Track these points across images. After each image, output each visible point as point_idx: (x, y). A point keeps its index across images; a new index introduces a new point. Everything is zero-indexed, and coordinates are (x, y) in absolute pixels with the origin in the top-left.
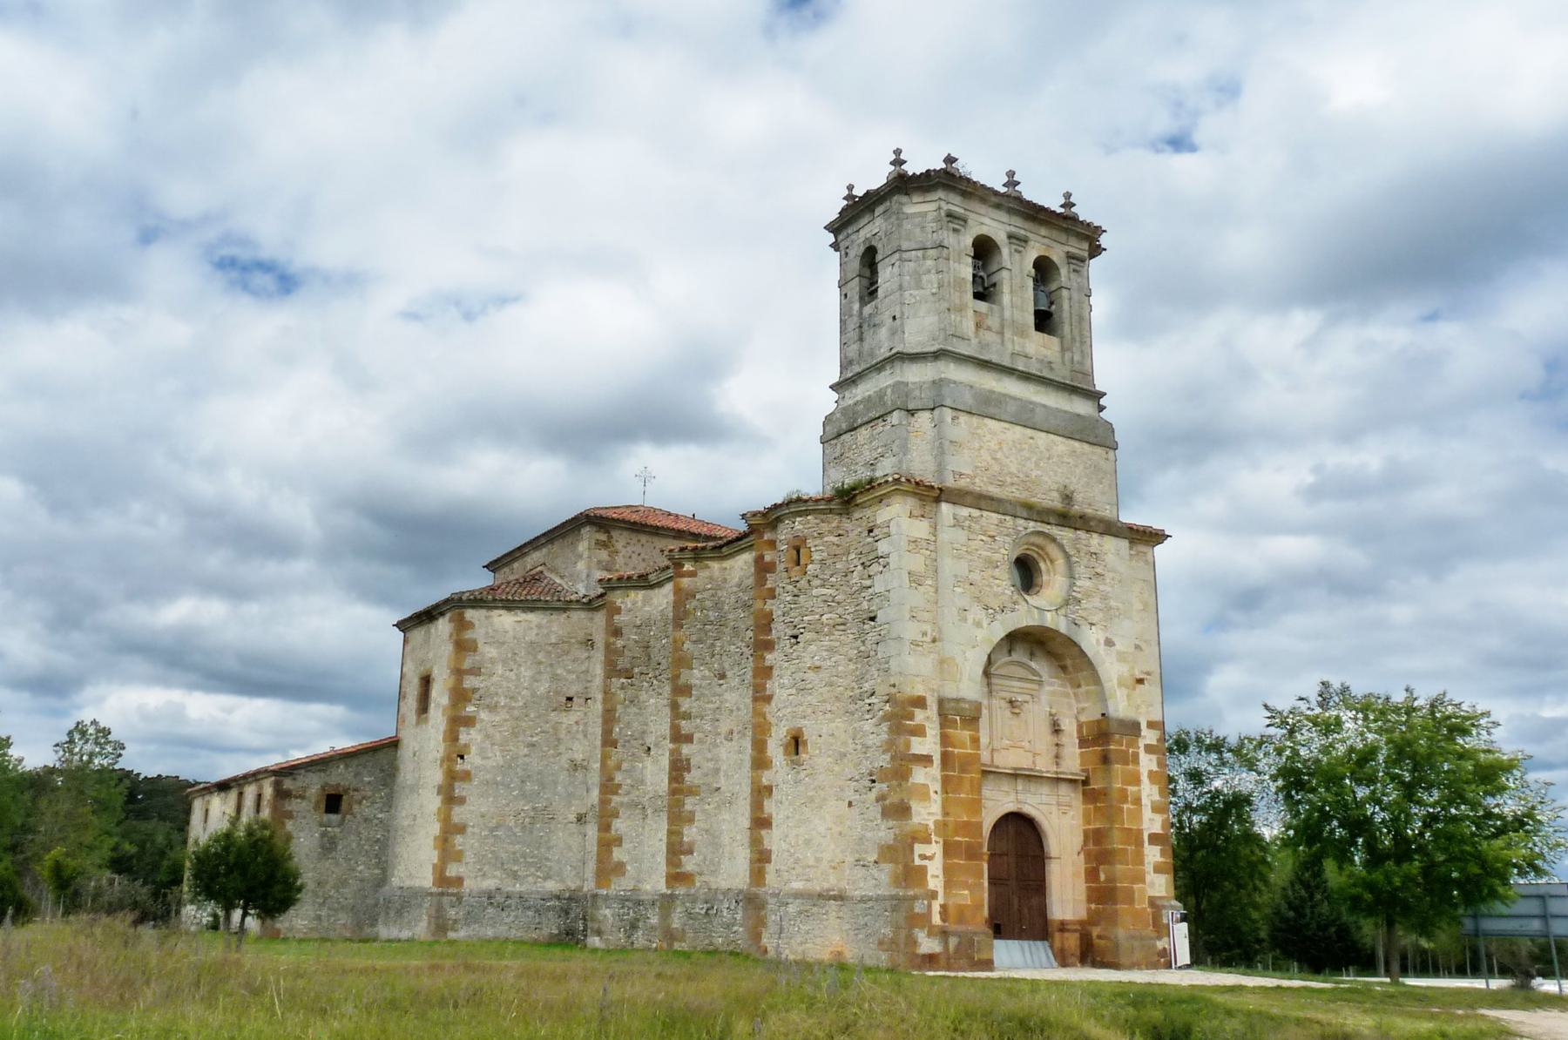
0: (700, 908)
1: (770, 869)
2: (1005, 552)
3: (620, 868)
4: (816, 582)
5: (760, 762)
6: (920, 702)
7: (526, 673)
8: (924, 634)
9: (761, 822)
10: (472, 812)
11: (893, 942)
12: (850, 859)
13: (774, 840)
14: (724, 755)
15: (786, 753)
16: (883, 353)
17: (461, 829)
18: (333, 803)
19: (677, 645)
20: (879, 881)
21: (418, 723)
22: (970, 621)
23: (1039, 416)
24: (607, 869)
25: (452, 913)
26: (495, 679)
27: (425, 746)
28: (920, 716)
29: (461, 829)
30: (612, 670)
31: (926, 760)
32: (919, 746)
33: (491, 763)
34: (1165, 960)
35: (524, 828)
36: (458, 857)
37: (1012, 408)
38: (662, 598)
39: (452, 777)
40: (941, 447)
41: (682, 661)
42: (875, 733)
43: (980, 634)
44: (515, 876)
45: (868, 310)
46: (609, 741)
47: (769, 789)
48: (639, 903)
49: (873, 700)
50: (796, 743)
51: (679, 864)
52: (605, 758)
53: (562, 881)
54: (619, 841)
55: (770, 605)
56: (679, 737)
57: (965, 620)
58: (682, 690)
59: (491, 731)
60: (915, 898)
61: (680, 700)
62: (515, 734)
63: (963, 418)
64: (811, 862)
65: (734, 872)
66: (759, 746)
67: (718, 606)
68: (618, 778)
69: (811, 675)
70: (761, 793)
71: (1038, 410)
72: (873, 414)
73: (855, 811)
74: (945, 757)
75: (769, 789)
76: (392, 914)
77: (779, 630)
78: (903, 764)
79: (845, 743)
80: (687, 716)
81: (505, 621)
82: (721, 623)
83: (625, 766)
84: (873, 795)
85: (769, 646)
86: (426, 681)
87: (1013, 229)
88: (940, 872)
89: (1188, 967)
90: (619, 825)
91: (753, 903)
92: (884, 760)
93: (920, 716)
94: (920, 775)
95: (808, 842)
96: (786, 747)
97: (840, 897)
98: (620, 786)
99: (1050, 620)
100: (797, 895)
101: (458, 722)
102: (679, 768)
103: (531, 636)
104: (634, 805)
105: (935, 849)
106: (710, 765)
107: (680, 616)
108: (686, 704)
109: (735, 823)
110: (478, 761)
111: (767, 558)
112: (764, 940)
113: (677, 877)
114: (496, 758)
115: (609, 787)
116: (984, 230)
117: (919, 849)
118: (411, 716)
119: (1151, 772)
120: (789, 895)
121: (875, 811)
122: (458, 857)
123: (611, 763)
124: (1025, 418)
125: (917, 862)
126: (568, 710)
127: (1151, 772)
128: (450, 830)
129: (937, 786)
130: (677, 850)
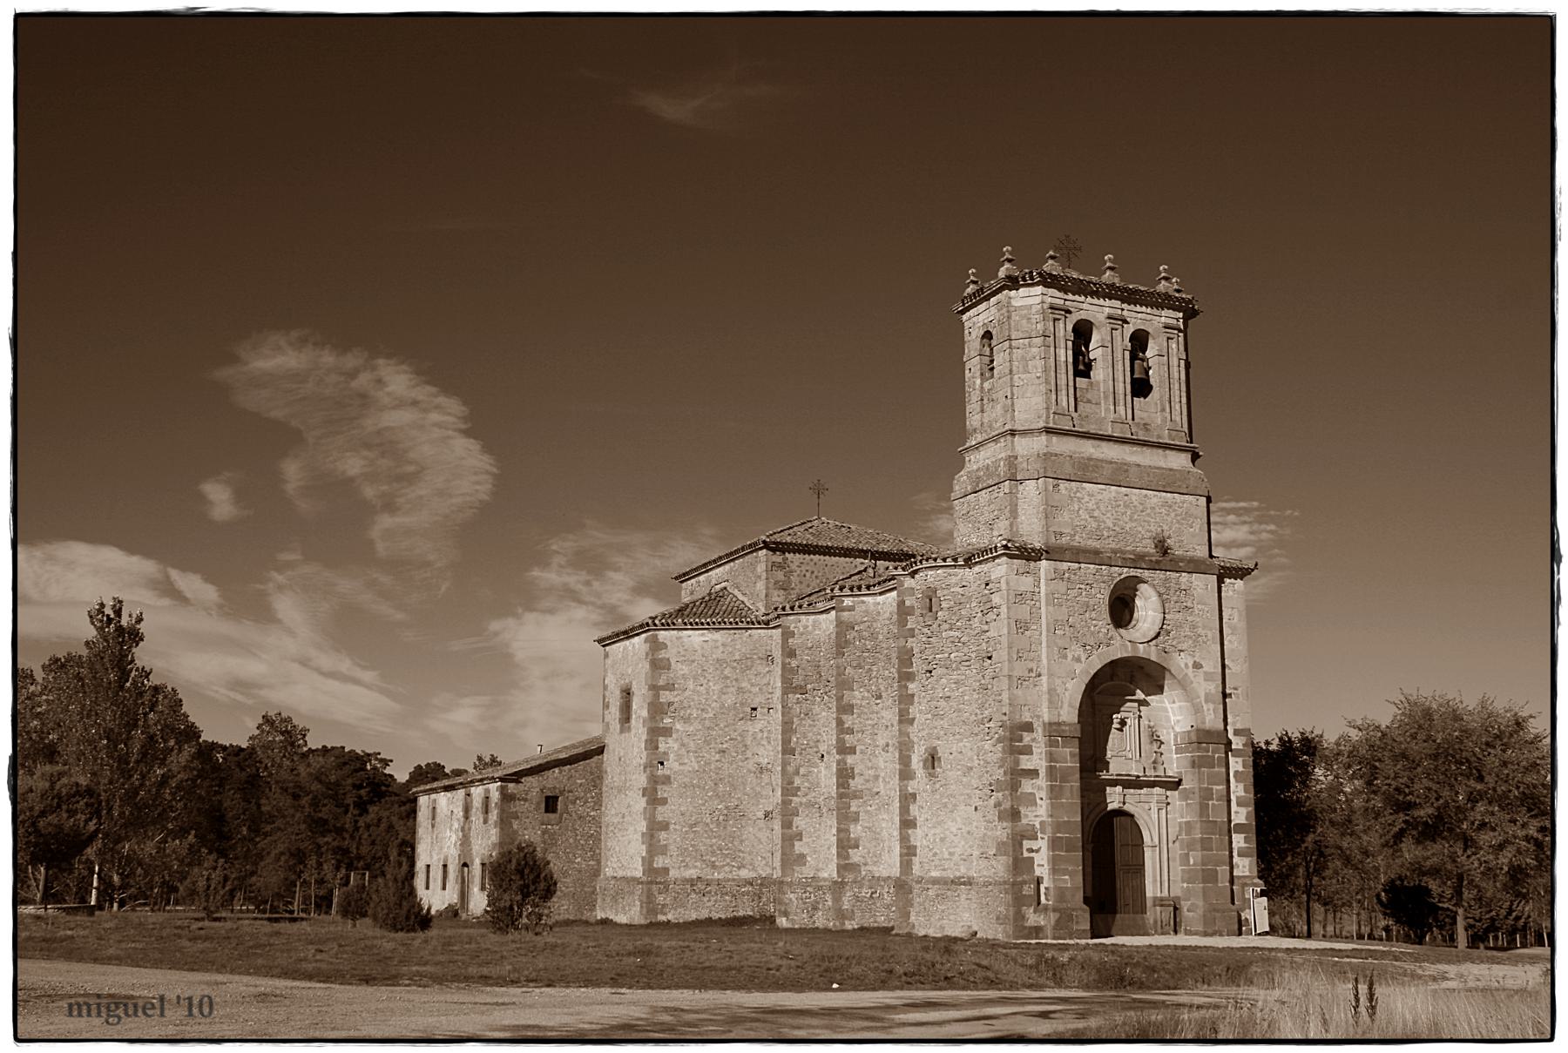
0: (865, 892)
1: (916, 860)
2: (1102, 597)
3: (801, 858)
4: (946, 626)
5: (906, 774)
6: (1028, 727)
7: (716, 688)
8: (1031, 670)
9: (907, 824)
10: (673, 811)
11: (1006, 917)
12: (976, 853)
13: (917, 837)
14: (882, 765)
15: (925, 767)
16: (998, 428)
17: (665, 826)
18: (551, 804)
19: (840, 673)
20: (999, 868)
21: (622, 731)
22: (1070, 657)
23: (1133, 478)
24: (791, 860)
25: (660, 899)
26: (687, 693)
27: (627, 753)
28: (1027, 737)
29: (665, 826)
30: (789, 687)
31: (1033, 773)
32: (1026, 763)
33: (687, 768)
34: (1240, 928)
35: (718, 825)
36: (664, 851)
37: (1107, 471)
38: (826, 624)
39: (654, 781)
40: (1050, 510)
41: (844, 684)
42: (994, 751)
43: (1078, 668)
44: (714, 866)
45: (987, 385)
46: (788, 750)
47: (914, 796)
48: (820, 888)
49: (991, 724)
50: (932, 759)
51: (848, 857)
52: (784, 764)
53: (754, 869)
54: (799, 836)
55: (911, 642)
56: (844, 749)
57: (1065, 657)
58: (845, 709)
59: (686, 740)
60: (1025, 882)
61: (844, 717)
62: (707, 743)
63: (1063, 485)
64: (946, 856)
65: (889, 866)
66: (905, 761)
67: (873, 636)
68: (797, 781)
69: (943, 703)
70: (907, 799)
71: (1133, 470)
72: (991, 482)
73: (979, 814)
74: (1051, 771)
75: (914, 796)
76: (608, 900)
77: (918, 666)
78: (1017, 775)
79: (971, 759)
80: (851, 731)
81: (695, 638)
82: (875, 650)
83: (802, 771)
84: (992, 801)
85: (910, 677)
86: (627, 693)
87: (1112, 311)
88: (1044, 862)
89: (1266, 933)
90: (799, 822)
91: (902, 887)
92: (999, 774)
93: (1027, 737)
94: (1027, 786)
95: (942, 840)
96: (925, 761)
97: (969, 882)
98: (798, 789)
99: (1142, 651)
100: (935, 881)
101: (656, 733)
102: (845, 775)
103: (718, 654)
104: (811, 805)
105: (1042, 844)
106: (871, 772)
107: (841, 643)
108: (849, 721)
109: (889, 825)
110: (676, 766)
111: (908, 603)
112: (912, 918)
113: (845, 867)
114: (692, 764)
115: (789, 790)
116: (1083, 315)
117: (1027, 844)
118: (615, 726)
119: (1236, 772)
120: (928, 882)
121: (993, 815)
122: (664, 851)
123: (790, 769)
124: (1119, 477)
125: (1026, 854)
126: (753, 718)
127: (1236, 772)
128: (655, 827)
129: (1043, 794)
130: (845, 844)
